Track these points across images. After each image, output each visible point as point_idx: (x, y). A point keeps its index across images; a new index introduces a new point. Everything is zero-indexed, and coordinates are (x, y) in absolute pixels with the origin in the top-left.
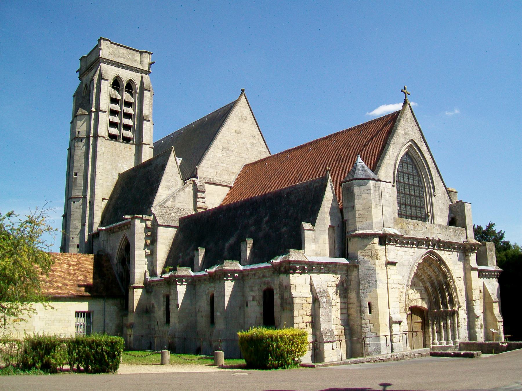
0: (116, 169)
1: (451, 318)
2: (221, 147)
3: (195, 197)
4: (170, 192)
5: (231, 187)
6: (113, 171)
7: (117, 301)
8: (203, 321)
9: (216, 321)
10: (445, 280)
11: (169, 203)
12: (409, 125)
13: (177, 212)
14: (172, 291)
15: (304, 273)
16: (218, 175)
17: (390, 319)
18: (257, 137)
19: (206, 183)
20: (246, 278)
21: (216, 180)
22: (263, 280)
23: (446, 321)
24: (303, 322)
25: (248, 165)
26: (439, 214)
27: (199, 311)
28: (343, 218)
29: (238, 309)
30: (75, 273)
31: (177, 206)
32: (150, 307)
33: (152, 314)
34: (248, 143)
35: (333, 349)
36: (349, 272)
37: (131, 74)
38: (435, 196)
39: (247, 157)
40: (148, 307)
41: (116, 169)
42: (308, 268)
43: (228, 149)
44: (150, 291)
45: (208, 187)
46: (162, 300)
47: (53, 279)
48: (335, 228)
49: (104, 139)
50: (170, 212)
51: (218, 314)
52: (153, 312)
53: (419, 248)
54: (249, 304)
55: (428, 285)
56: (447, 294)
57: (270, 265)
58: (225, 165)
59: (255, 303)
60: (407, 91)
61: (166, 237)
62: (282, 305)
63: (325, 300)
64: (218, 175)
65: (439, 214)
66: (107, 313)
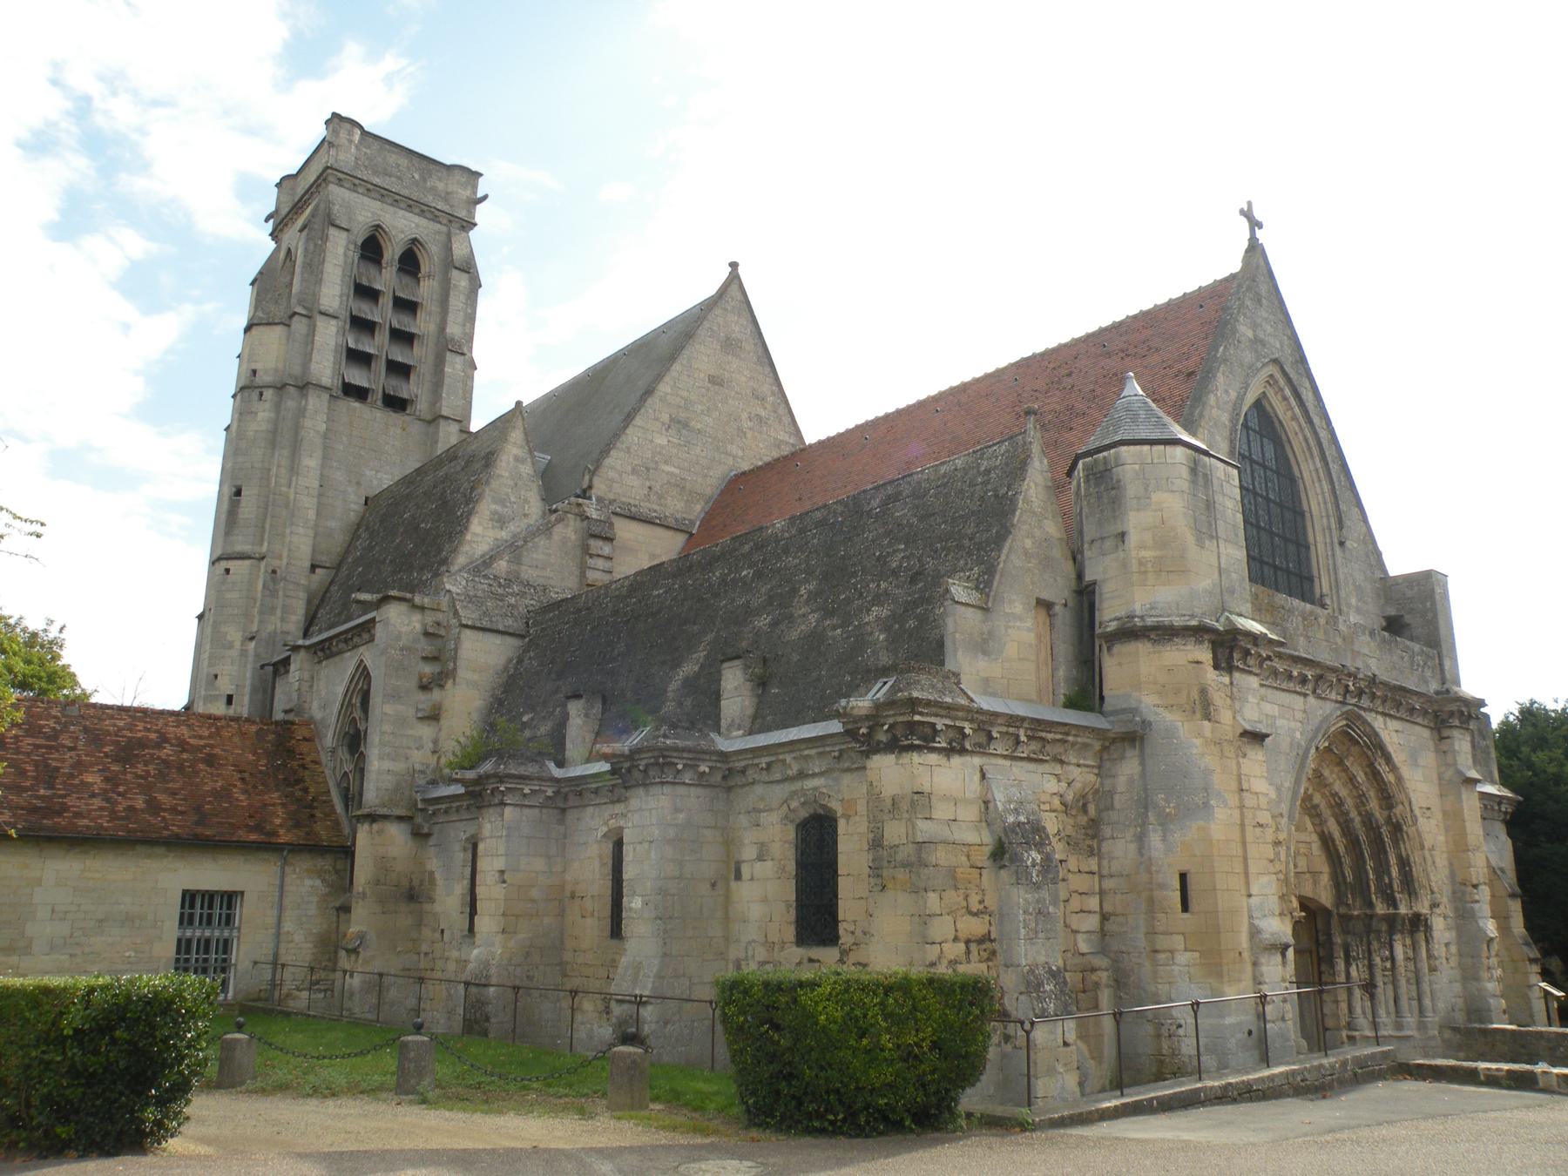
0: (358, 483)
1: (1408, 942)
2: (665, 418)
3: (586, 551)
4: (504, 534)
5: (691, 535)
6: (350, 489)
7: (325, 863)
8: (589, 928)
9: (628, 927)
10: (1386, 813)
11: (502, 566)
12: (1265, 315)
13: (522, 595)
14: (488, 826)
15: (962, 751)
17: (1255, 932)
19: (615, 514)
20: (739, 780)
21: (645, 508)
22: (797, 785)
23: (1391, 947)
24: (956, 939)
25: (744, 473)
26: (1353, 601)
28: (1080, 576)
29: (704, 888)
30: (196, 773)
31: (524, 576)
32: (422, 882)
33: (427, 907)
34: (745, 416)
35: (1066, 1044)
36: (1107, 764)
38: (1342, 544)
39: (740, 453)
40: (416, 883)
41: (358, 483)
42: (973, 733)
43: (686, 425)
44: (426, 830)
45: (626, 531)
46: (460, 857)
47: (118, 785)
48: (1058, 609)
50: (500, 591)
52: (431, 900)
53: (1319, 697)
54: (746, 871)
55: (1333, 828)
56: (1393, 860)
57: (835, 727)
58: (677, 471)
59: (766, 869)
60: (1258, 215)
61: (482, 657)
62: (876, 870)
63: (1036, 855)
65: (1353, 601)
66: (287, 901)
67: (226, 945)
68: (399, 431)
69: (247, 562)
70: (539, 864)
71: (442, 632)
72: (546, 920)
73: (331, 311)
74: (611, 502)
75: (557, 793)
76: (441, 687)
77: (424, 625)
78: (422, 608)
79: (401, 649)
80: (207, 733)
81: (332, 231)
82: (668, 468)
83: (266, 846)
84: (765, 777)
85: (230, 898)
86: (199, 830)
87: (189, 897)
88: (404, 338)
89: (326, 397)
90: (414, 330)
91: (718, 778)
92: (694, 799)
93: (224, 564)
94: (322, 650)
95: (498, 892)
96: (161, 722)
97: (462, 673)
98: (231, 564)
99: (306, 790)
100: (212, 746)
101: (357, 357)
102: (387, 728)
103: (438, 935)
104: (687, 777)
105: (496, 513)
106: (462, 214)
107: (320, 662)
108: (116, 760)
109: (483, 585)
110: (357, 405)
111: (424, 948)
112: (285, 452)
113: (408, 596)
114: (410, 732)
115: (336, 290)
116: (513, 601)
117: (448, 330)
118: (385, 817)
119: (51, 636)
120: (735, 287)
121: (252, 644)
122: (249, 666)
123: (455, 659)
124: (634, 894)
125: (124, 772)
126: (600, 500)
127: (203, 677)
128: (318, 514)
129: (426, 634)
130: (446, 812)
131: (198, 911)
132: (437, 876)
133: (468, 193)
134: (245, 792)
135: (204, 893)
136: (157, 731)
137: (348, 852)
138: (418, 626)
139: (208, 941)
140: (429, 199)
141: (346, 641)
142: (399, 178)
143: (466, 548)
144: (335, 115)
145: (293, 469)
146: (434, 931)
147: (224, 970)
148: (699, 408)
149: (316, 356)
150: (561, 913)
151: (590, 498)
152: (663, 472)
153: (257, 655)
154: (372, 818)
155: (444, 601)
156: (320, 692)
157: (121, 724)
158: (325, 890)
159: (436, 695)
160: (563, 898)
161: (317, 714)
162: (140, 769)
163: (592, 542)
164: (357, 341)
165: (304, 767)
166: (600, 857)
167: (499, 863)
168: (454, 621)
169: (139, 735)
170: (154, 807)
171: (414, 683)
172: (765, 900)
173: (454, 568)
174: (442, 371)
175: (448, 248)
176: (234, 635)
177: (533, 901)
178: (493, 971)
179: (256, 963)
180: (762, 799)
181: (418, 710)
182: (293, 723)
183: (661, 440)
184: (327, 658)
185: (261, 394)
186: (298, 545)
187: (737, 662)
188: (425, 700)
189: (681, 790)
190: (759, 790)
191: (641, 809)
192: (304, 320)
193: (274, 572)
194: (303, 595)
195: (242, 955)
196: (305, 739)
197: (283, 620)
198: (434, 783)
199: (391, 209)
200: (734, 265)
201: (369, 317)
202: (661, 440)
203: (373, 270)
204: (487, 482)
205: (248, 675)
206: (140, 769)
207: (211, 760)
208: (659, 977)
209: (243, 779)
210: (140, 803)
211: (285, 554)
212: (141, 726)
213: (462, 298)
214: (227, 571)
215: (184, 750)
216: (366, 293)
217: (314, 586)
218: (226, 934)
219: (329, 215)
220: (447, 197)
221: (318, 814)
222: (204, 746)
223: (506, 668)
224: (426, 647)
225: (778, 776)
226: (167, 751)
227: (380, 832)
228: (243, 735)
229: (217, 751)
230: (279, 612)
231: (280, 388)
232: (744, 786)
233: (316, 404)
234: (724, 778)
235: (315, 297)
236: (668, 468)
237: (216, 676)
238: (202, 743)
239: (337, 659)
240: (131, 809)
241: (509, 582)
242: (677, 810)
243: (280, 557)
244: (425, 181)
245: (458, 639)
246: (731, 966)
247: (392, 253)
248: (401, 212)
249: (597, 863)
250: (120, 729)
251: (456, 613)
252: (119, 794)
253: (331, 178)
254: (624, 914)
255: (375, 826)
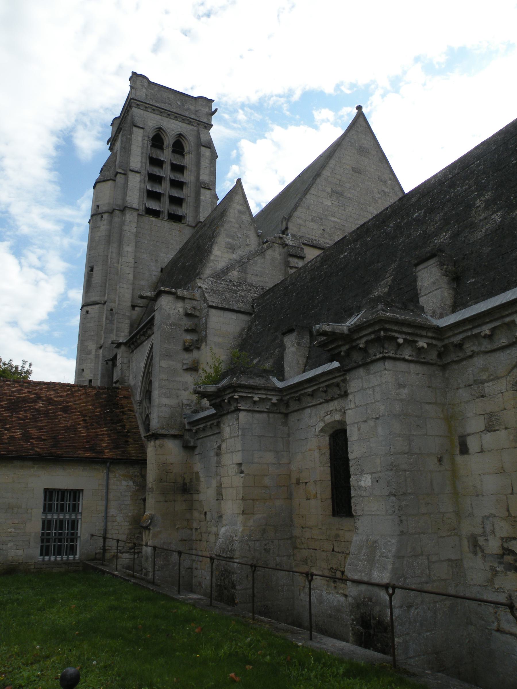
0: (157, 261)
2: (329, 190)
4: (235, 256)
6: (152, 264)
8: (314, 507)
11: (234, 274)
16: (326, 236)
18: (390, 182)
19: (304, 244)
27: (298, 482)
31: (249, 280)
33: (195, 497)
34: (375, 191)
37: (181, 127)
40: (187, 481)
41: (157, 261)
43: (342, 195)
44: (192, 444)
47: (6, 424)
49: (135, 214)
51: (366, 481)
52: (198, 492)
54: (473, 444)
58: (339, 221)
61: (224, 329)
64: (326, 236)
66: (111, 496)
67: (74, 524)
68: (178, 232)
69: (97, 306)
70: (269, 457)
71: (197, 314)
72: (278, 503)
73: (136, 169)
74: (301, 237)
75: (280, 401)
76: (198, 348)
77: (185, 309)
78: (183, 299)
79: (171, 325)
80: (65, 394)
81: (135, 129)
82: (333, 219)
83: (95, 460)
84: (486, 345)
85: (75, 494)
86: (54, 450)
87: (49, 493)
88: (178, 185)
89: (135, 214)
90: (182, 180)
91: (433, 356)
92: (414, 375)
93: (85, 309)
94: (133, 344)
95: (238, 480)
96: (38, 389)
97: (212, 338)
98: (89, 308)
99: (124, 426)
100: (67, 402)
101: (153, 195)
102: (163, 376)
103: (203, 516)
104: (407, 353)
105: (228, 243)
106: (205, 120)
107: (133, 351)
108: (8, 409)
109: (223, 285)
110: (153, 219)
111: (195, 525)
112: (115, 245)
113: (174, 290)
114: (178, 379)
115: (139, 159)
116: (243, 294)
117: (201, 178)
118: (164, 436)
119: (26, 369)
120: (361, 119)
121: (101, 351)
122: (100, 363)
123: (206, 328)
124: (362, 472)
125: (11, 417)
126: (293, 236)
127: (80, 372)
128: (134, 277)
129: (188, 315)
130: (204, 429)
131: (68, 502)
132: (201, 475)
133: (207, 110)
134: (85, 427)
135: (58, 491)
136: (35, 393)
137: (142, 463)
138: (181, 310)
139: (61, 521)
140: (187, 114)
141: (144, 335)
142: (170, 104)
143: (211, 264)
144: (134, 73)
145: (120, 254)
146: (200, 513)
147: (72, 540)
148: (348, 185)
149: (129, 193)
150: (290, 497)
151: (287, 235)
152: (328, 223)
153: (104, 356)
154: (156, 436)
155: (198, 294)
156: (132, 369)
157: (14, 389)
158: (135, 488)
159: (195, 354)
160: (290, 485)
161: (132, 382)
162: (22, 414)
163: (291, 259)
164: (152, 187)
165: (123, 413)
166: (319, 448)
167: (238, 458)
168: (205, 305)
169: (24, 395)
170: (26, 437)
171: (180, 347)
172: (502, 471)
173: (204, 276)
174: (199, 199)
175: (198, 137)
176: (92, 346)
177: (266, 487)
178: (236, 545)
179: (92, 535)
180: (484, 369)
181: (184, 364)
182: (118, 388)
183: (328, 203)
184: (136, 348)
185: (102, 217)
186: (125, 294)
187: (432, 261)
188: (188, 358)
189: (402, 366)
190: (479, 361)
191: (363, 389)
192: (123, 176)
193: (112, 310)
194: (127, 321)
195: (83, 531)
196: (125, 397)
197: (117, 336)
198: (196, 412)
199: (166, 119)
200: (359, 108)
201: (158, 174)
202: (328, 203)
203: (159, 152)
204: (222, 225)
205: (100, 368)
206: (22, 414)
207: (66, 410)
208: (398, 557)
209: (85, 420)
210: (18, 434)
211: (117, 299)
212: (26, 390)
213: (207, 161)
214: (87, 312)
215: (50, 404)
216: (156, 162)
217: (134, 317)
218: (73, 517)
219: (133, 122)
220: (196, 112)
221: (131, 440)
222: (63, 402)
223: (240, 335)
224: (187, 323)
225: (504, 341)
226: (40, 404)
227: (161, 446)
228: (87, 395)
229: (71, 404)
230: (115, 332)
231: (111, 212)
232: (461, 360)
233: (130, 217)
234: (440, 355)
235: (128, 163)
236: (333, 219)
237: (83, 370)
238: (61, 400)
239: (140, 347)
240: (12, 438)
241: (240, 284)
242: (401, 386)
243: (114, 302)
244: (183, 105)
245: (207, 316)
246: (465, 543)
247: (169, 141)
248: (172, 121)
249: (317, 454)
250: (13, 392)
251: (205, 300)
252: (6, 429)
253: (133, 105)
254: (353, 493)
255: (158, 442)
